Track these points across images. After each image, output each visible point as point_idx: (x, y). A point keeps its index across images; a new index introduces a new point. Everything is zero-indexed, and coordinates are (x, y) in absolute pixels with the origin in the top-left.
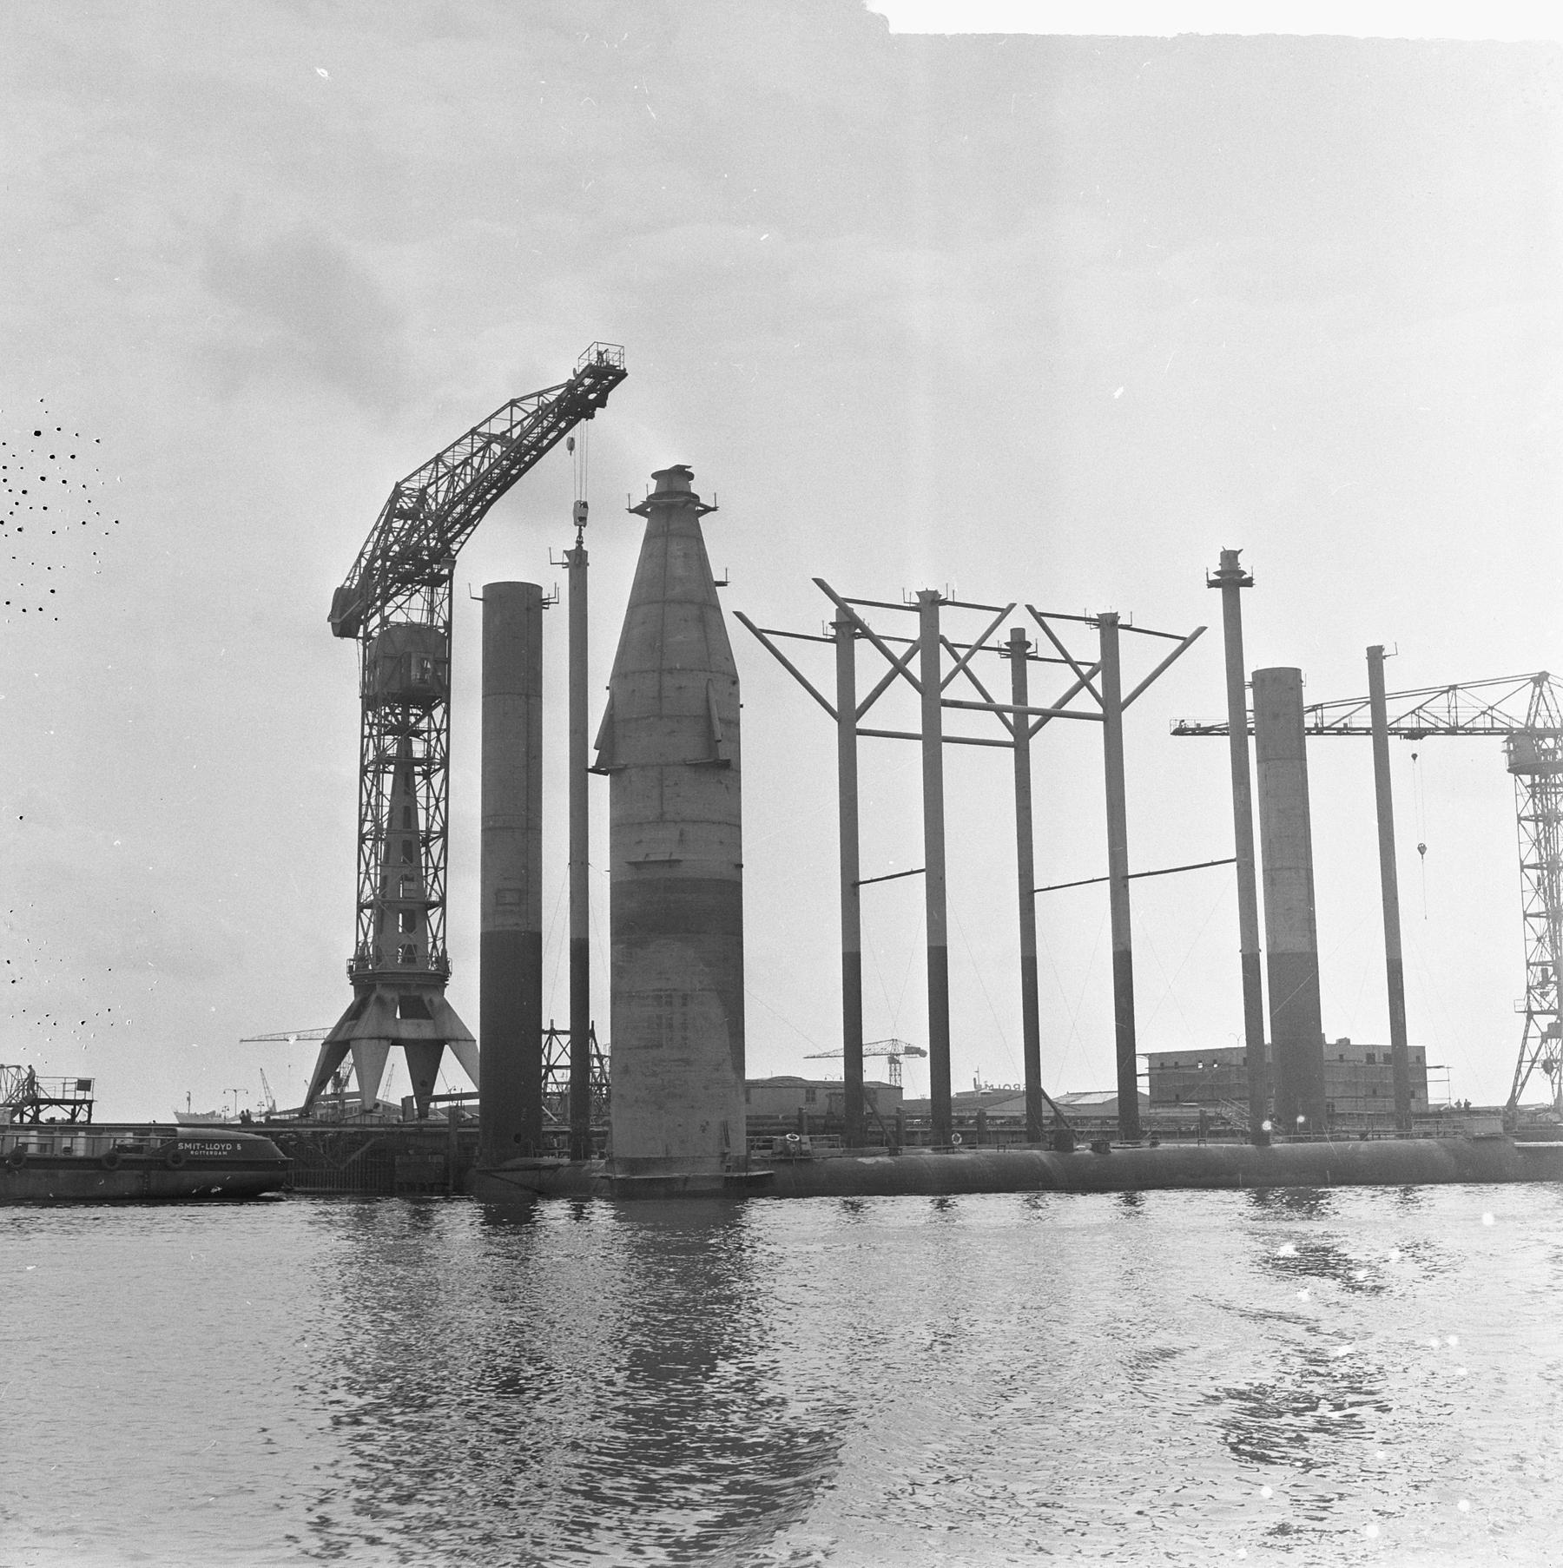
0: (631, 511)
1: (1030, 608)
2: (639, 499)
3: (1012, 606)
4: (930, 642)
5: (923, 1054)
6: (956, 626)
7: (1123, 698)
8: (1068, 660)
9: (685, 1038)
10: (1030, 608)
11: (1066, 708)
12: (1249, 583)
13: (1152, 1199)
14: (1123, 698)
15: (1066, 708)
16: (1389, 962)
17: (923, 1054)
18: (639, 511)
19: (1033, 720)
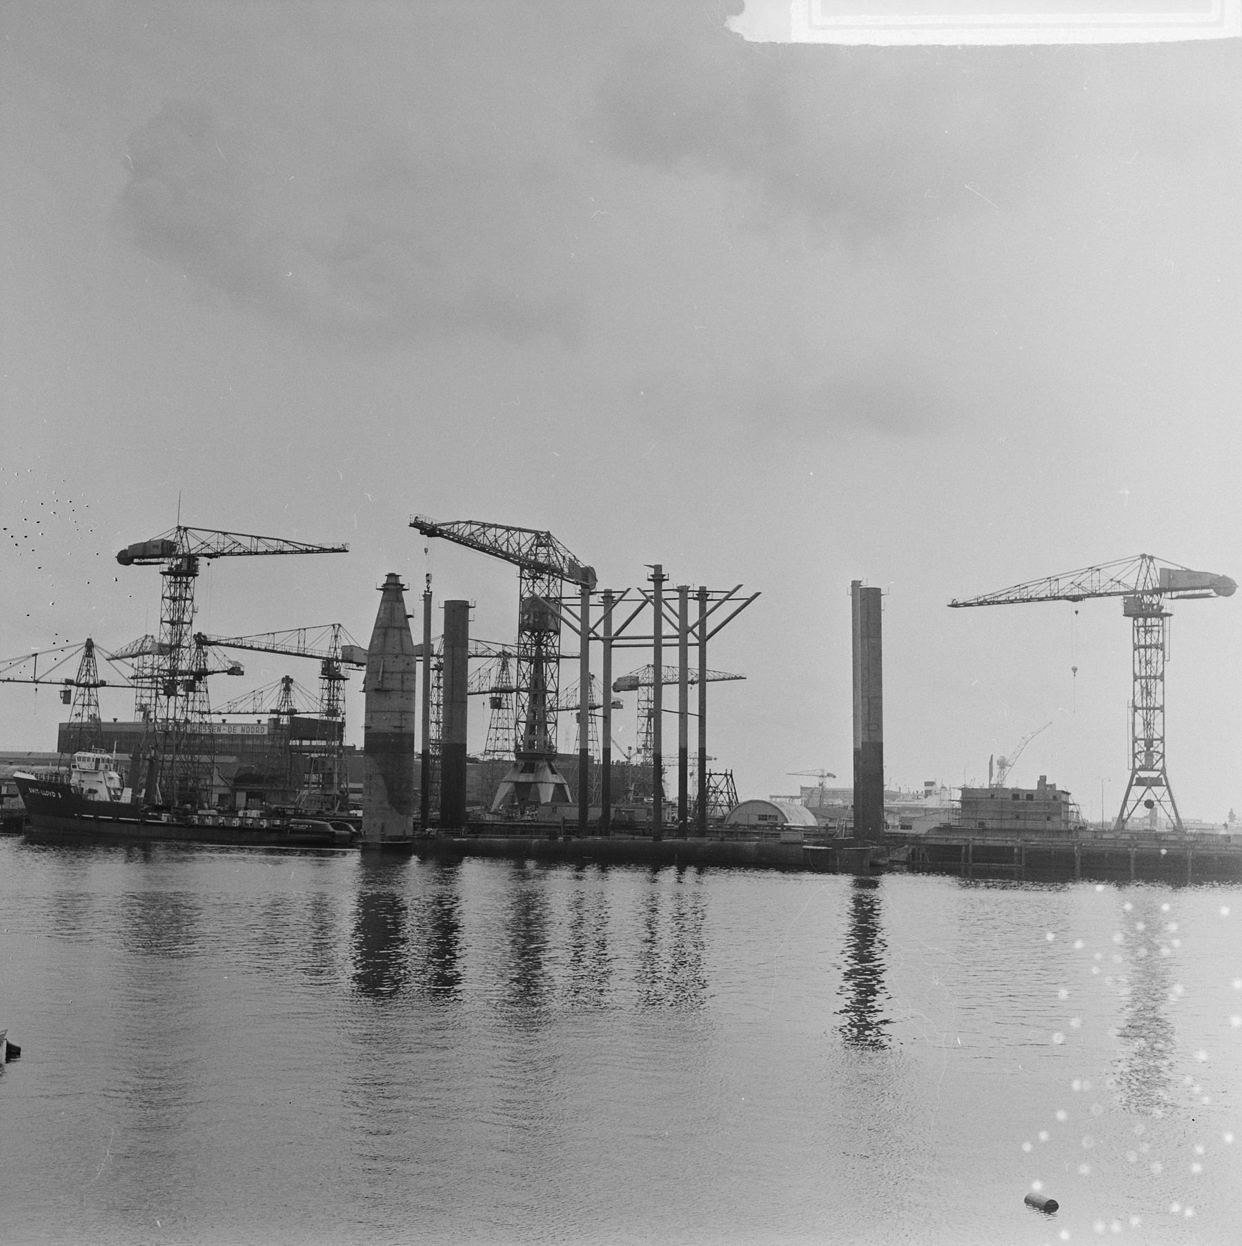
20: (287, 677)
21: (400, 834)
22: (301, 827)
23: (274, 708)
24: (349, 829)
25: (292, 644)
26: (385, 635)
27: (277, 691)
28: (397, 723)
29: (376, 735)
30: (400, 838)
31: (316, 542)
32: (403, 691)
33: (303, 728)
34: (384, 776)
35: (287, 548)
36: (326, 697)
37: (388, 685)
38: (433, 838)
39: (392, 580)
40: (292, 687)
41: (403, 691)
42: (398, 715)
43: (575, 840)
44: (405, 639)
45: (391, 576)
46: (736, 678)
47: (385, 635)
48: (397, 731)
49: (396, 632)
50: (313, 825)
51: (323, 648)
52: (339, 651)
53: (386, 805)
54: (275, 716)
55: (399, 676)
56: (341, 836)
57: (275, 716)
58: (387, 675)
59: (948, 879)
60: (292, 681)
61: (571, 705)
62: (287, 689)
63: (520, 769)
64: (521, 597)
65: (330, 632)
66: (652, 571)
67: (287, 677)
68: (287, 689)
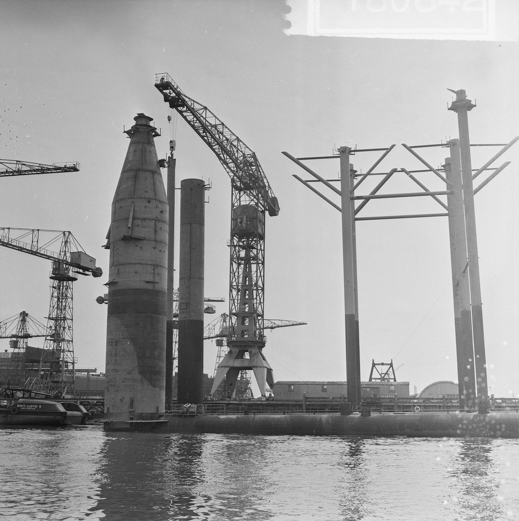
0: (449, 109)
1: (404, 145)
2: (128, 128)
3: (393, 146)
4: (349, 174)
5: (97, 273)
6: (360, 163)
7: (474, 188)
8: (431, 170)
9: (116, 360)
10: (404, 145)
11: (378, 194)
12: (157, 135)
13: (369, 446)
14: (474, 188)
15: (378, 194)
16: (201, 222)
17: (97, 273)
18: (128, 132)
19: (357, 203)
20: (24, 312)
21: (153, 411)
22: (30, 407)
23: (14, 333)
24: (80, 411)
25: (26, 242)
26: (136, 177)
27: (16, 322)
28: (150, 278)
29: (124, 292)
30: (152, 416)
31: (48, 162)
32: (155, 240)
33: (33, 355)
34: (133, 340)
35: (25, 168)
36: (55, 294)
37: (138, 233)
38: (192, 415)
39: (143, 122)
40: (27, 319)
41: (155, 240)
42: (150, 269)
43: (374, 415)
44: (158, 183)
45: (140, 117)
46: (301, 324)
47: (136, 177)
48: (150, 287)
49: (148, 175)
50: (42, 404)
51: (55, 249)
52: (68, 255)
53: (138, 377)
54: (15, 339)
55: (152, 223)
56: (73, 417)
57: (15, 339)
58: (138, 222)
59: (307, 437)
60: (27, 315)
61: (212, 335)
62: (24, 321)
63: (235, 355)
64: (233, 205)
65: (62, 239)
66: (454, 97)
67: (24, 312)
68: (24, 321)
